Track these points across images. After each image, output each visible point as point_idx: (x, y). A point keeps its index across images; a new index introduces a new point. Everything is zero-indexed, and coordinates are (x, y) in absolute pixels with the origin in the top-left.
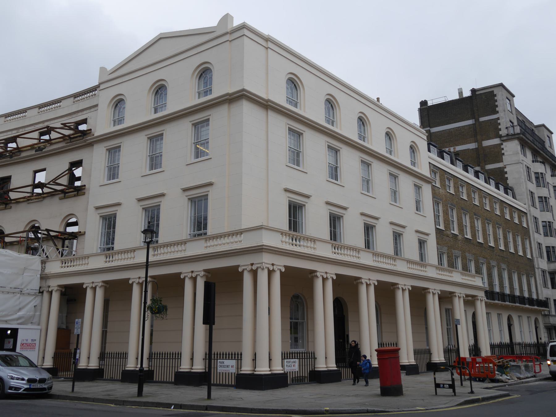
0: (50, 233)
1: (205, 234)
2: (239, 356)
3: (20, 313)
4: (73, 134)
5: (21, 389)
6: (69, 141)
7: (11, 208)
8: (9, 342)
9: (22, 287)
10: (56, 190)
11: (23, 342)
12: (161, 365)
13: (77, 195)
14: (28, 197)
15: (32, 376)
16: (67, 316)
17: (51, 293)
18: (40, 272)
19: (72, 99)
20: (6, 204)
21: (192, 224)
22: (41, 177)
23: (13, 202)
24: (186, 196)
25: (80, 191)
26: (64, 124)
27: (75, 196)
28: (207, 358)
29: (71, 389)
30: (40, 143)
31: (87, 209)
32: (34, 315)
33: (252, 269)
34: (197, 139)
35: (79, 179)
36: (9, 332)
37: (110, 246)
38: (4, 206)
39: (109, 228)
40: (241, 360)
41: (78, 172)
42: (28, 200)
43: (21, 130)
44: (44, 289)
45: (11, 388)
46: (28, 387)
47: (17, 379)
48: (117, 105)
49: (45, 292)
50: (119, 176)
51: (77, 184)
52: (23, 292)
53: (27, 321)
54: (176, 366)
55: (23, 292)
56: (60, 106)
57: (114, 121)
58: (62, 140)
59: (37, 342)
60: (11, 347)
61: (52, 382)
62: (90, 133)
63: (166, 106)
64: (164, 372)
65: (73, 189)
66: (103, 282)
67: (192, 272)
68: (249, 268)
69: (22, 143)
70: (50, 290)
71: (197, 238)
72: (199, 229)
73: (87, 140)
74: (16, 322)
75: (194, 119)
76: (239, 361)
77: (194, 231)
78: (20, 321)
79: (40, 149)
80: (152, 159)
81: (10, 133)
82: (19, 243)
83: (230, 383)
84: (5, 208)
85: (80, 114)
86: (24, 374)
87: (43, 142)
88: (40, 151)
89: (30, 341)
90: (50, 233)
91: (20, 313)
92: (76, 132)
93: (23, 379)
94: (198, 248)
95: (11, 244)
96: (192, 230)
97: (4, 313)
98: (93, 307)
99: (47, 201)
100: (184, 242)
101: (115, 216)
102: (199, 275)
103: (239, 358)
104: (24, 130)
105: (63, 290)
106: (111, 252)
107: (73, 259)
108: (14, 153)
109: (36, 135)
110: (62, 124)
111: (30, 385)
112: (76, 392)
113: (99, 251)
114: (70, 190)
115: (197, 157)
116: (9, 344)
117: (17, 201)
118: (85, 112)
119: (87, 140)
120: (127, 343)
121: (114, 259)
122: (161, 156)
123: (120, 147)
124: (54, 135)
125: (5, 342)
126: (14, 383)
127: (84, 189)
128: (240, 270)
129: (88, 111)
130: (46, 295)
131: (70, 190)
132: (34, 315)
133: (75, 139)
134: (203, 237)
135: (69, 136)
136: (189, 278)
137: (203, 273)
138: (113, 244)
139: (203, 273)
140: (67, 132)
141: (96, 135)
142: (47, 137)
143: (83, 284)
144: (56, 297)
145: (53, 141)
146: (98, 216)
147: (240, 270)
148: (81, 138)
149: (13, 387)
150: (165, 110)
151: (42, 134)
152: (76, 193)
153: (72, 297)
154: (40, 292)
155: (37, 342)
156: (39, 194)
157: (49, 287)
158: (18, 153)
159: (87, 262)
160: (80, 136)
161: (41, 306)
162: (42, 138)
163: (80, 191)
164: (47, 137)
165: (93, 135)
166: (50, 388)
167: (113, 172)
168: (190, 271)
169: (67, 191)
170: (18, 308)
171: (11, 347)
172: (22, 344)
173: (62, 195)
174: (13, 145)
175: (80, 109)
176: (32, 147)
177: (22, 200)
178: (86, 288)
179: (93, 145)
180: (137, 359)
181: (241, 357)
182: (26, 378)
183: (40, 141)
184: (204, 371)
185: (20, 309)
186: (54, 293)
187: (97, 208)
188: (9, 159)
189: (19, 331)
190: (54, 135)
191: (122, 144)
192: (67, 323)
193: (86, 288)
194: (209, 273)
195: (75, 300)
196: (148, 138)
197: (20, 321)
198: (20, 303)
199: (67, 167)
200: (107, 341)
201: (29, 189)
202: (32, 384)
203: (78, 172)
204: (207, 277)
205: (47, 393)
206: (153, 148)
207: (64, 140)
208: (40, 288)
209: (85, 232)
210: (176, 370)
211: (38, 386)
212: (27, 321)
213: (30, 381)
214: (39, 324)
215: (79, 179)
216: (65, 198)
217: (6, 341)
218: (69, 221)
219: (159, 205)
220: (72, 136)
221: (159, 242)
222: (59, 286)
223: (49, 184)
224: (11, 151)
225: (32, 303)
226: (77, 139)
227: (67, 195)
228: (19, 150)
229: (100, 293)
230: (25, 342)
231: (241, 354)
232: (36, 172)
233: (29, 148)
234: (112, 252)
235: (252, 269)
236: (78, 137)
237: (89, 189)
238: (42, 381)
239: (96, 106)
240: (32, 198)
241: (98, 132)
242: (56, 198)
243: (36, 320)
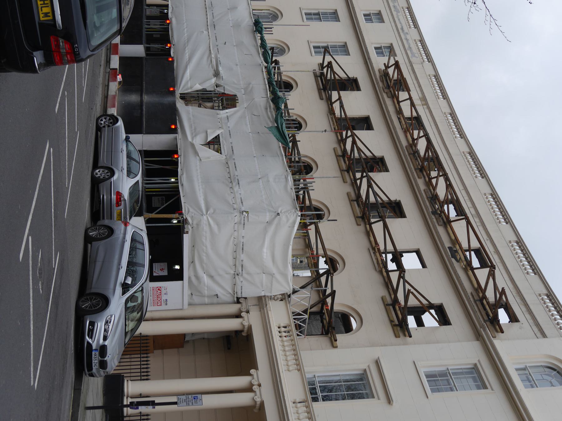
0: (330, 298)
1: (315, 400)
2: (145, 378)
3: (205, 279)
4: (488, 303)
5: (91, 338)
6: (476, 298)
7: (358, 225)
8: (162, 270)
9: (245, 275)
10: (396, 291)
11: (163, 290)
12: (132, 367)
13: (393, 326)
14: (379, 249)
15: (109, 351)
16: (204, 338)
17: (238, 316)
18: (269, 294)
19: (545, 292)
20: (363, 218)
21: (327, 379)
22: (410, 262)
23: (368, 226)
24: (369, 366)
25: (400, 328)
26: (503, 292)
27: (391, 321)
29: (90, 404)
30: (464, 251)
31: (373, 345)
32: (204, 296)
33: (253, 385)
34: (454, 374)
35: (420, 323)
36: (177, 267)
37: (320, 395)
38: (359, 215)
39: (349, 388)
40: (141, 380)
41: (429, 319)
42: (374, 249)
43: (477, 220)
44: (244, 304)
45: (92, 324)
46: (94, 347)
47: (105, 330)
48: (555, 370)
49: (238, 306)
50: (437, 394)
51: (411, 321)
52: (237, 277)
53: (195, 290)
54: (132, 375)
55: (237, 277)
57: (525, 369)
58: (476, 286)
59: (163, 307)
60: (155, 274)
61: (101, 376)
62: (497, 331)
63: (532, 387)
65: (401, 314)
66: (262, 403)
67: (259, 385)
68: (255, 382)
69: (460, 228)
70: (243, 314)
71: (307, 388)
72: (323, 389)
73: (485, 330)
74: (192, 274)
75: (484, 367)
76: (139, 378)
77: (319, 382)
78: (193, 279)
79: (454, 253)
80: (444, 374)
81: (470, 205)
82: (308, 245)
84: (356, 217)
85: (524, 309)
86: (112, 341)
87: (465, 257)
88: (451, 255)
89: (164, 297)
90: (330, 298)
91: (205, 279)
92: (493, 305)
93: (105, 338)
94: (293, 390)
95: (306, 236)
96: (321, 379)
97: (204, 258)
99: (376, 278)
100: (300, 369)
101: (370, 395)
102: (244, 320)
103: (143, 378)
104: (479, 224)
105: (244, 334)
106: (295, 332)
108: (440, 216)
109: (475, 244)
110: (503, 288)
111: (96, 350)
112: (85, 414)
113: (308, 376)
114: (399, 312)
115: (427, 376)
116: (160, 270)
117: (369, 233)
118: (528, 316)
119: (485, 330)
120: (164, 377)
121: (285, 339)
122: (452, 390)
123: (485, 387)
124: (482, 275)
125: (162, 264)
126: (100, 326)
127: (405, 335)
128: (252, 371)
129: (531, 321)
130: (234, 309)
131: (399, 312)
132: (204, 296)
133: (481, 307)
134: (309, 397)
135: (485, 297)
136: (242, 323)
137: (258, 400)
138: (325, 399)
139: (258, 400)
140: (490, 294)
141: (496, 342)
142: (476, 263)
143: (256, 368)
144: (232, 324)
145: (470, 273)
146: (364, 366)
147: (252, 371)
148: (486, 318)
149: (93, 326)
150: (526, 387)
151: (478, 252)
152: (397, 323)
153: (234, 350)
154: (238, 299)
155: (163, 307)
156: (384, 261)
157: (248, 312)
158: (441, 223)
159: (291, 368)
160: (488, 315)
161: (218, 304)
162: (473, 253)
163: (400, 328)
164: (476, 263)
165: (494, 337)
166: (92, 375)
167: (440, 381)
168: (261, 382)
169: (397, 308)
170: (213, 273)
171: (155, 274)
172: (159, 289)
173: (389, 301)
174: (453, 214)
175: (532, 307)
176: (455, 241)
177: (372, 239)
178: (250, 375)
179: (478, 340)
180: (141, 396)
181: (143, 380)
182: (106, 343)
183: (466, 251)
184: (125, 414)
185: (211, 277)
186: (239, 320)
187: (377, 363)
188: (430, 210)
189: (180, 282)
190: (482, 275)
191: (489, 390)
192: (194, 341)
193: (250, 375)
194: (260, 409)
195: (229, 349)
196: (475, 365)
197: (193, 279)
198: (219, 275)
199: (435, 301)
201: (390, 247)
202: (97, 353)
203: (429, 319)
204: (254, 407)
205: (84, 370)
206: (460, 373)
207: (476, 290)
208: (246, 298)
209: (337, 347)
211: (95, 361)
212: (195, 290)
213: (103, 350)
214: (190, 304)
215: (420, 323)
216: (386, 305)
217: (164, 265)
218: (352, 319)
219: (373, 397)
220: (484, 302)
221: (315, 404)
222: (250, 328)
223: (405, 281)
224: (443, 212)
225: (222, 291)
226: (482, 310)
227: (391, 307)
228: (447, 222)
230: (163, 291)
231: (147, 379)
232: (418, 252)
233: (453, 238)
234: (310, 400)
235: (253, 385)
236: (486, 314)
237: (406, 344)
238: (103, 365)
239: (544, 335)
240: (378, 254)
241: (500, 344)
242: (383, 292)
243: (196, 299)
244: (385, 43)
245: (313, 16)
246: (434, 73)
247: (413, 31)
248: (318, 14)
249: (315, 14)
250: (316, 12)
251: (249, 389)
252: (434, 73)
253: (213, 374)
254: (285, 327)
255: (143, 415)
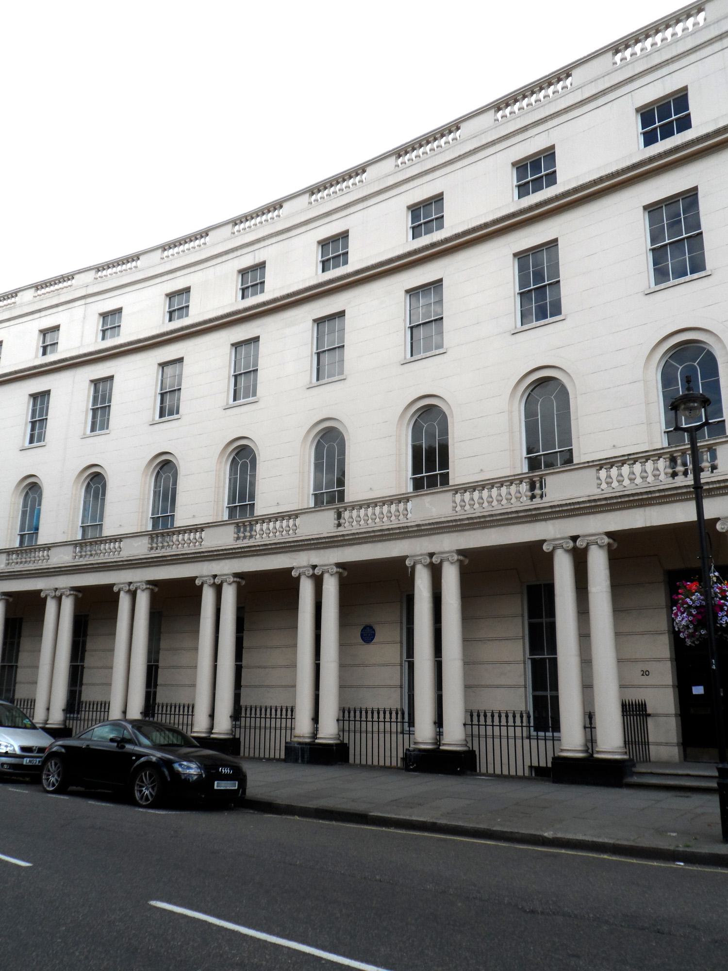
28: (532, 724)
33: (214, 583)
40: (192, 715)
56: (136, 267)
64: (381, 746)
76: (190, 717)
83: (370, 763)
94: (322, 524)
98: (132, 624)
107: (250, 522)
193: (202, 584)
194: (344, 569)
200: (159, 682)
210: (406, 746)
229: (143, 600)
231: (193, 708)
235: (214, 583)
244: (237, 281)
245: (36, 432)
246: (93, 272)
247: (79, 280)
248: (33, 424)
249: (33, 429)
250: (29, 426)
251: (318, 582)
252: (230, 226)
253: (113, 634)
254: (239, 531)
255: (344, 717)
